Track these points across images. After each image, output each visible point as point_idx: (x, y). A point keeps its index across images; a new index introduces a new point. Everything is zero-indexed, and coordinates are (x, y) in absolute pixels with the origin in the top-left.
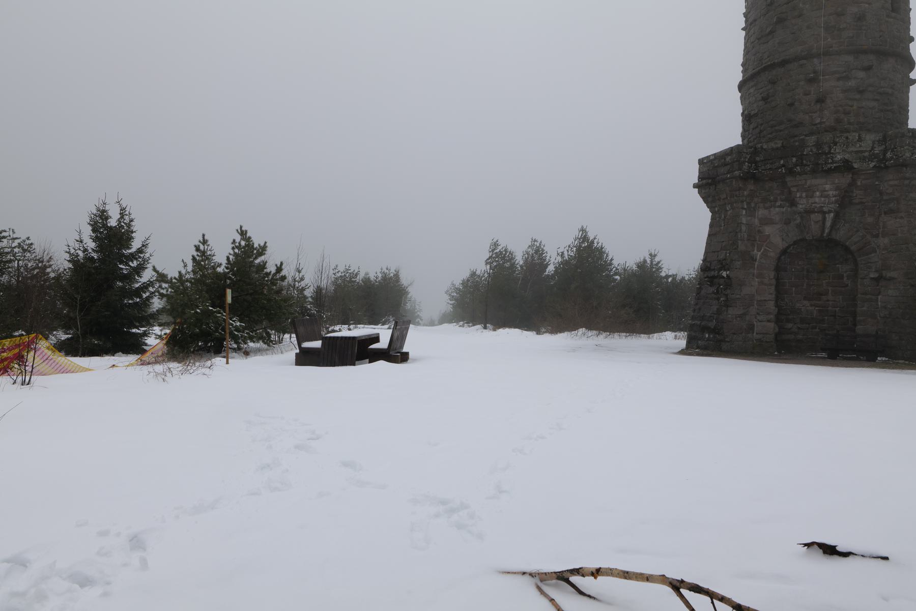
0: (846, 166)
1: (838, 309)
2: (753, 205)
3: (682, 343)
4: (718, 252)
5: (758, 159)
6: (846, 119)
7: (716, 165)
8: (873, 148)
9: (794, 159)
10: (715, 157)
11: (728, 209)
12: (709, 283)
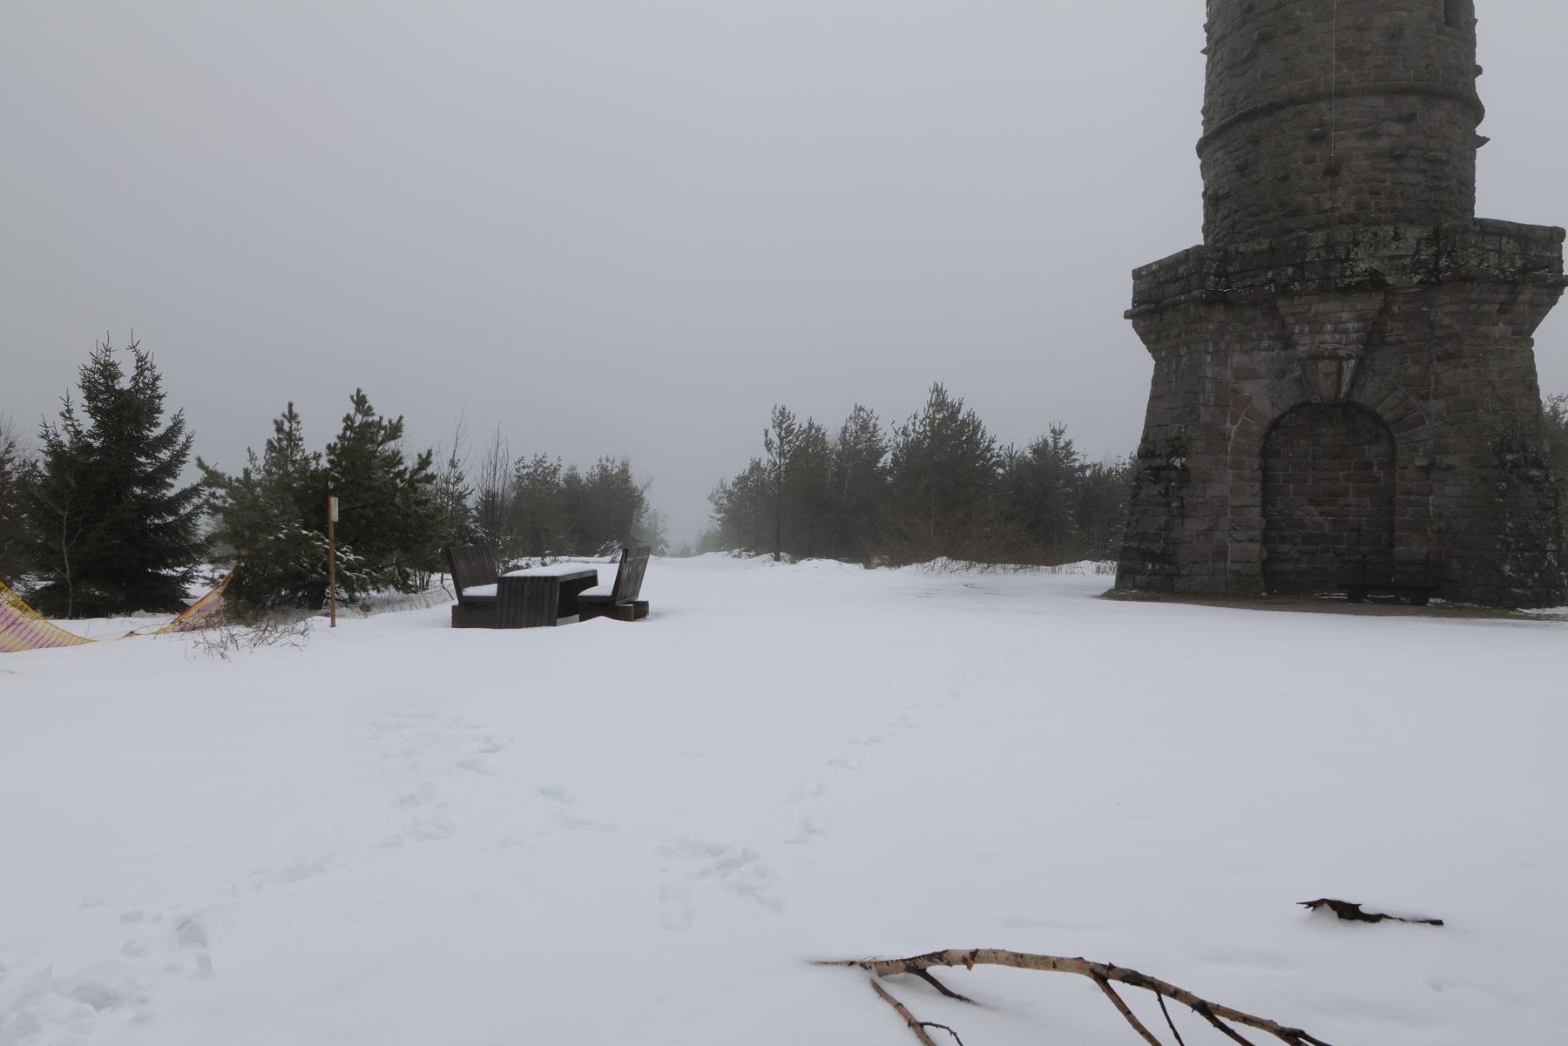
0: (1375, 282)
2: (1223, 346)
3: (1110, 580)
4: (1167, 425)
5: (1231, 269)
9: (1290, 270)
11: (1182, 353)
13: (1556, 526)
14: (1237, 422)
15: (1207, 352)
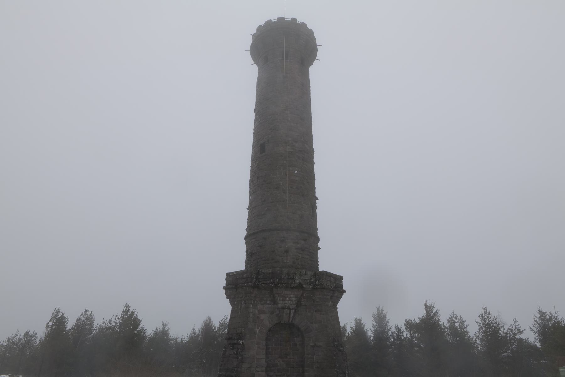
0: (300, 287)
1: (295, 363)
2: (256, 302)
4: (237, 328)
5: (259, 277)
6: (297, 262)
7: (238, 278)
8: (311, 278)
9: (278, 280)
10: (237, 273)
11: (242, 303)
15: (251, 304)
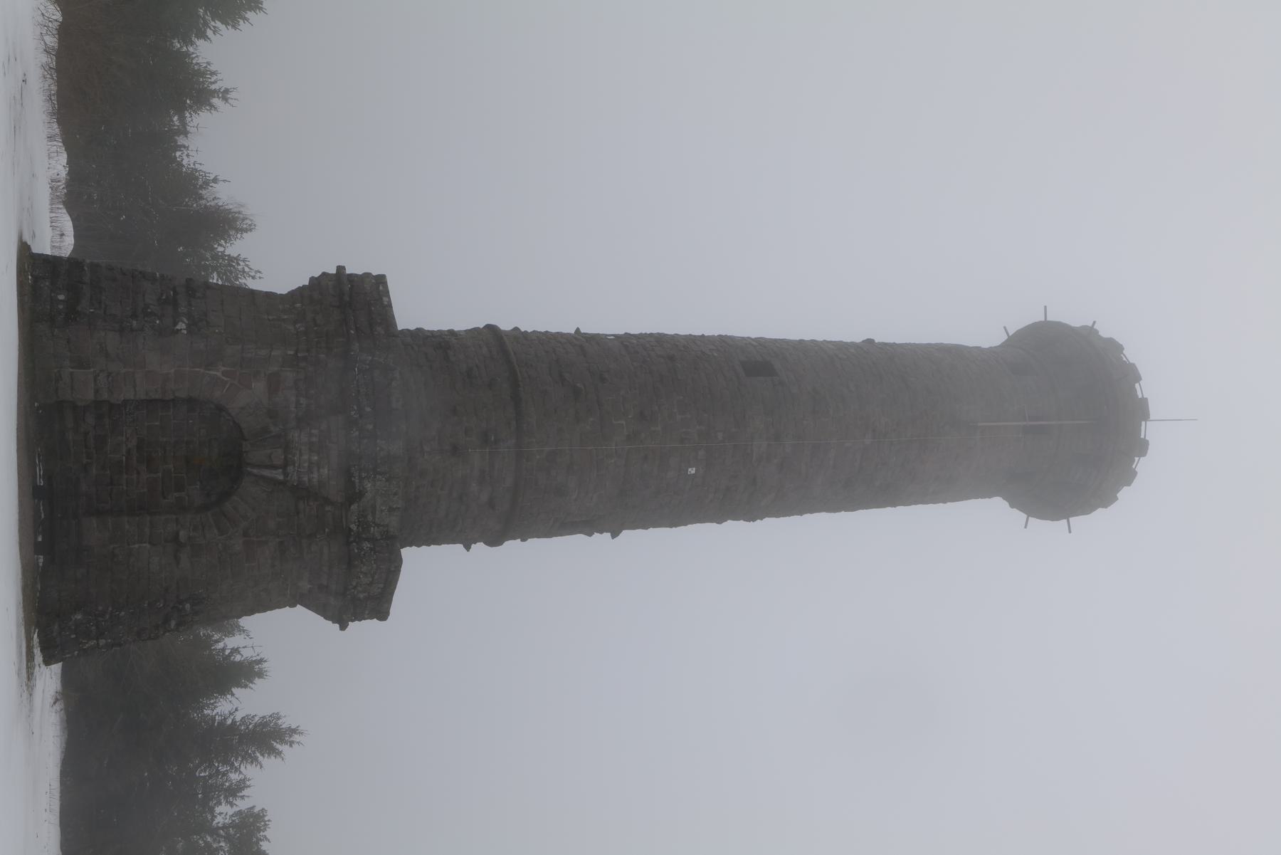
3: (44, 245)
9: (370, 427)
11: (297, 326)
12: (164, 297)
13: (122, 642)
14: (224, 376)
